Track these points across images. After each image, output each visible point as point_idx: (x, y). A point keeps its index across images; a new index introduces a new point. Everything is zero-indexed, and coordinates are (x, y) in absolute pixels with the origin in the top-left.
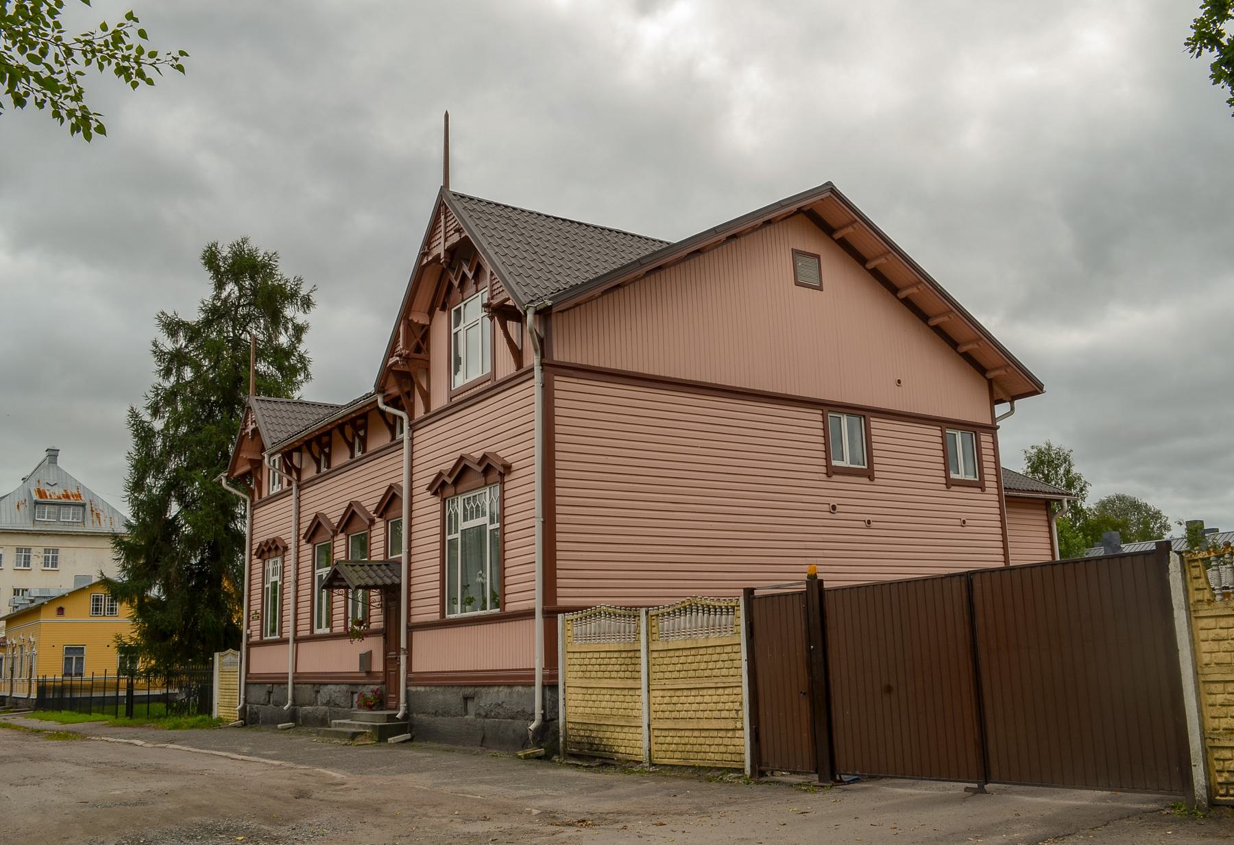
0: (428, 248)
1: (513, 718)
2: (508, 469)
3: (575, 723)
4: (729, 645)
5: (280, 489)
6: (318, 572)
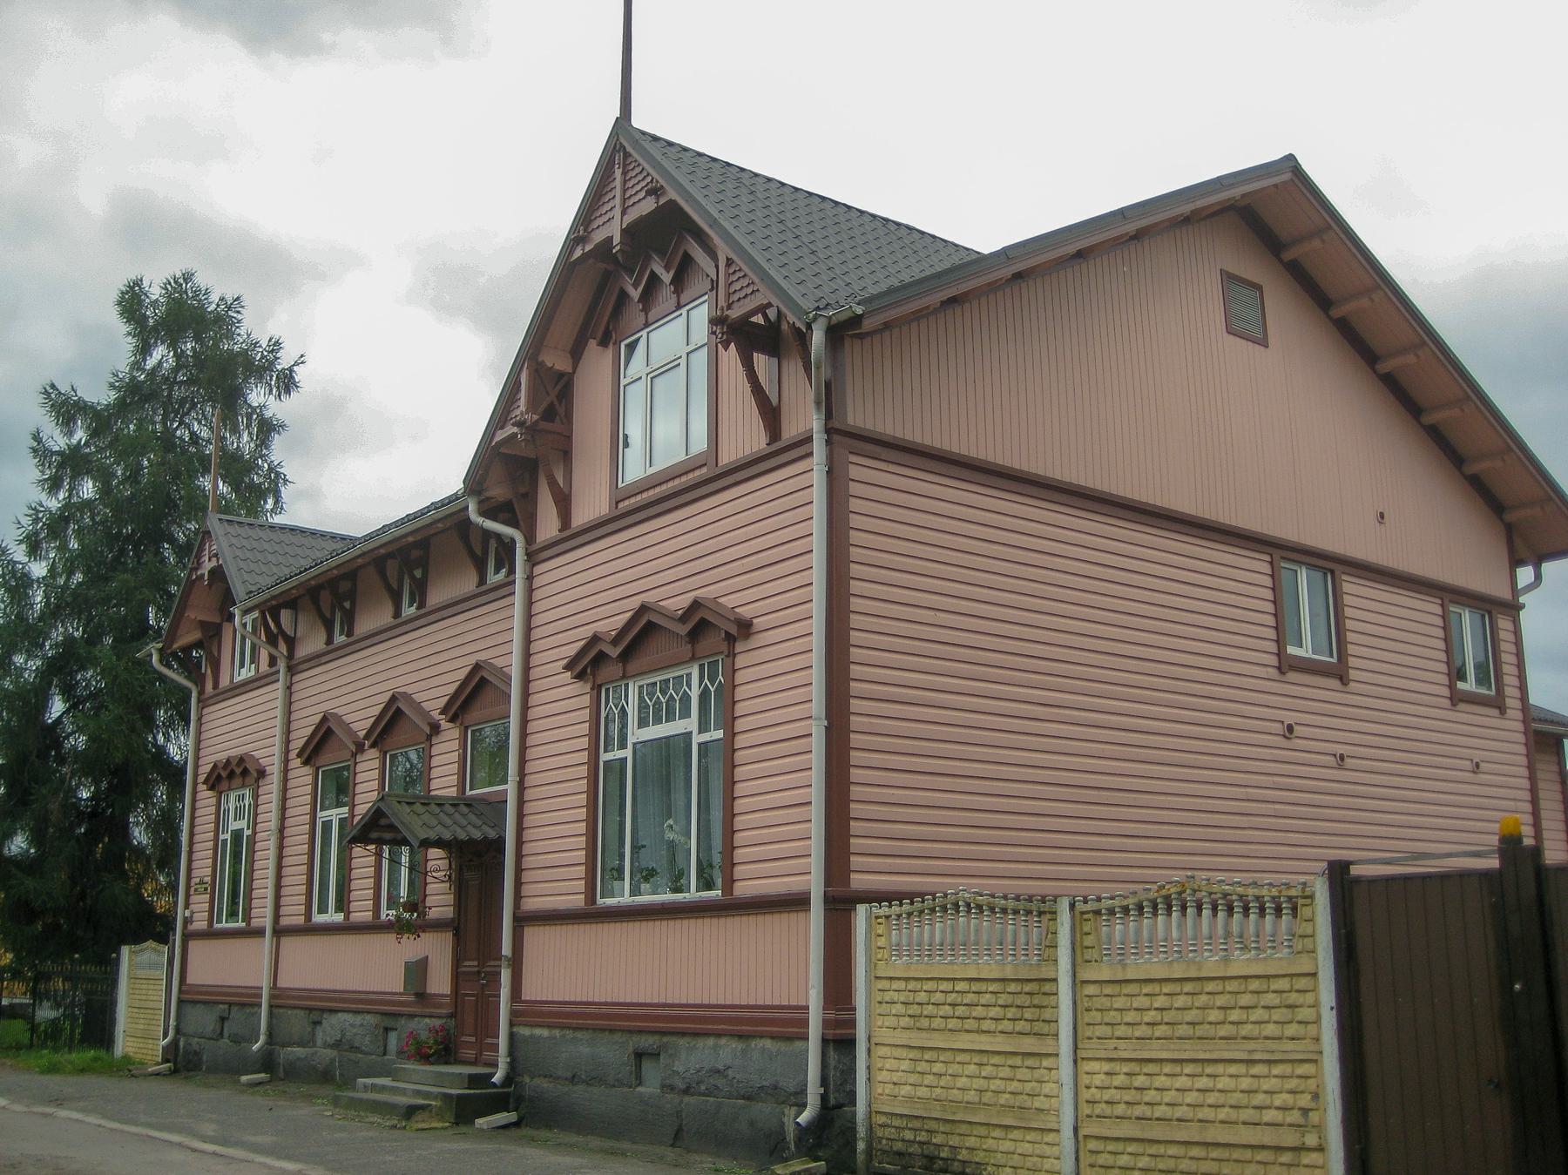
0: (585, 231)
1: (749, 1098)
2: (745, 628)
3: (892, 1114)
4: (1284, 976)
5: (253, 673)
6: (323, 815)
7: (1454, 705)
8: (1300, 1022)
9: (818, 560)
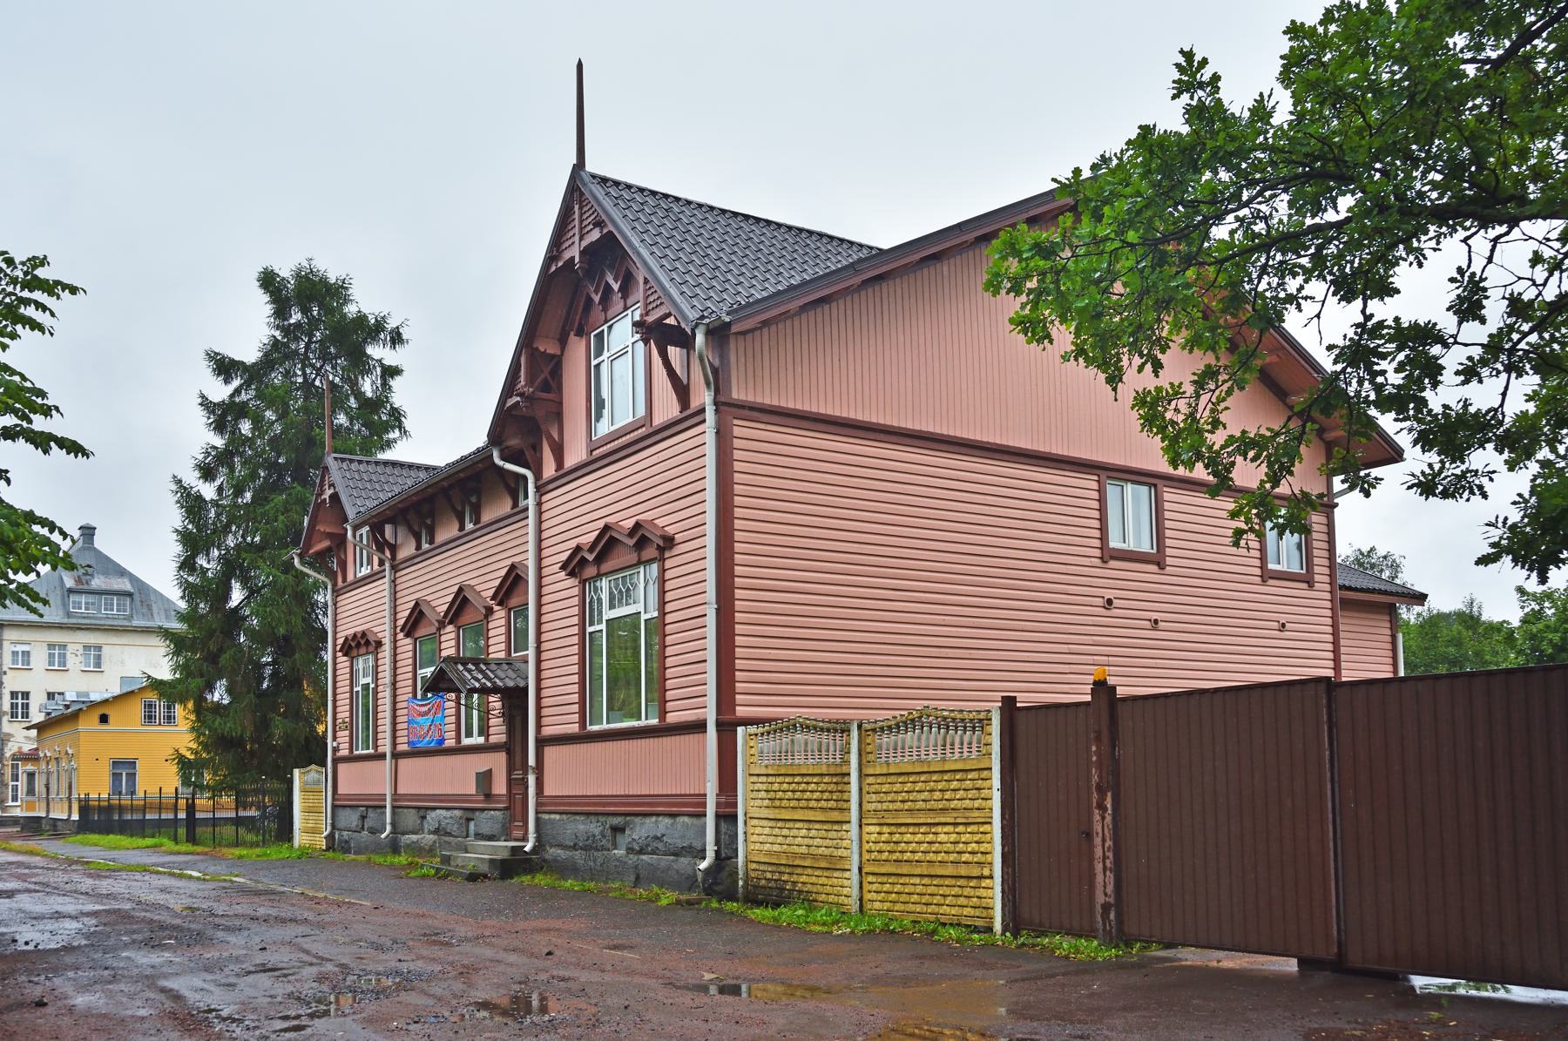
1: (675, 854)
5: (369, 571)
7: (1263, 581)
8: (983, 799)
9: (710, 495)
